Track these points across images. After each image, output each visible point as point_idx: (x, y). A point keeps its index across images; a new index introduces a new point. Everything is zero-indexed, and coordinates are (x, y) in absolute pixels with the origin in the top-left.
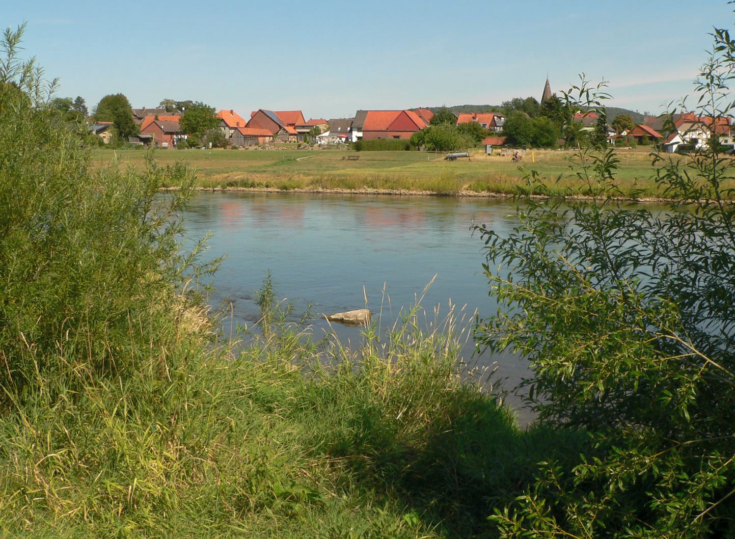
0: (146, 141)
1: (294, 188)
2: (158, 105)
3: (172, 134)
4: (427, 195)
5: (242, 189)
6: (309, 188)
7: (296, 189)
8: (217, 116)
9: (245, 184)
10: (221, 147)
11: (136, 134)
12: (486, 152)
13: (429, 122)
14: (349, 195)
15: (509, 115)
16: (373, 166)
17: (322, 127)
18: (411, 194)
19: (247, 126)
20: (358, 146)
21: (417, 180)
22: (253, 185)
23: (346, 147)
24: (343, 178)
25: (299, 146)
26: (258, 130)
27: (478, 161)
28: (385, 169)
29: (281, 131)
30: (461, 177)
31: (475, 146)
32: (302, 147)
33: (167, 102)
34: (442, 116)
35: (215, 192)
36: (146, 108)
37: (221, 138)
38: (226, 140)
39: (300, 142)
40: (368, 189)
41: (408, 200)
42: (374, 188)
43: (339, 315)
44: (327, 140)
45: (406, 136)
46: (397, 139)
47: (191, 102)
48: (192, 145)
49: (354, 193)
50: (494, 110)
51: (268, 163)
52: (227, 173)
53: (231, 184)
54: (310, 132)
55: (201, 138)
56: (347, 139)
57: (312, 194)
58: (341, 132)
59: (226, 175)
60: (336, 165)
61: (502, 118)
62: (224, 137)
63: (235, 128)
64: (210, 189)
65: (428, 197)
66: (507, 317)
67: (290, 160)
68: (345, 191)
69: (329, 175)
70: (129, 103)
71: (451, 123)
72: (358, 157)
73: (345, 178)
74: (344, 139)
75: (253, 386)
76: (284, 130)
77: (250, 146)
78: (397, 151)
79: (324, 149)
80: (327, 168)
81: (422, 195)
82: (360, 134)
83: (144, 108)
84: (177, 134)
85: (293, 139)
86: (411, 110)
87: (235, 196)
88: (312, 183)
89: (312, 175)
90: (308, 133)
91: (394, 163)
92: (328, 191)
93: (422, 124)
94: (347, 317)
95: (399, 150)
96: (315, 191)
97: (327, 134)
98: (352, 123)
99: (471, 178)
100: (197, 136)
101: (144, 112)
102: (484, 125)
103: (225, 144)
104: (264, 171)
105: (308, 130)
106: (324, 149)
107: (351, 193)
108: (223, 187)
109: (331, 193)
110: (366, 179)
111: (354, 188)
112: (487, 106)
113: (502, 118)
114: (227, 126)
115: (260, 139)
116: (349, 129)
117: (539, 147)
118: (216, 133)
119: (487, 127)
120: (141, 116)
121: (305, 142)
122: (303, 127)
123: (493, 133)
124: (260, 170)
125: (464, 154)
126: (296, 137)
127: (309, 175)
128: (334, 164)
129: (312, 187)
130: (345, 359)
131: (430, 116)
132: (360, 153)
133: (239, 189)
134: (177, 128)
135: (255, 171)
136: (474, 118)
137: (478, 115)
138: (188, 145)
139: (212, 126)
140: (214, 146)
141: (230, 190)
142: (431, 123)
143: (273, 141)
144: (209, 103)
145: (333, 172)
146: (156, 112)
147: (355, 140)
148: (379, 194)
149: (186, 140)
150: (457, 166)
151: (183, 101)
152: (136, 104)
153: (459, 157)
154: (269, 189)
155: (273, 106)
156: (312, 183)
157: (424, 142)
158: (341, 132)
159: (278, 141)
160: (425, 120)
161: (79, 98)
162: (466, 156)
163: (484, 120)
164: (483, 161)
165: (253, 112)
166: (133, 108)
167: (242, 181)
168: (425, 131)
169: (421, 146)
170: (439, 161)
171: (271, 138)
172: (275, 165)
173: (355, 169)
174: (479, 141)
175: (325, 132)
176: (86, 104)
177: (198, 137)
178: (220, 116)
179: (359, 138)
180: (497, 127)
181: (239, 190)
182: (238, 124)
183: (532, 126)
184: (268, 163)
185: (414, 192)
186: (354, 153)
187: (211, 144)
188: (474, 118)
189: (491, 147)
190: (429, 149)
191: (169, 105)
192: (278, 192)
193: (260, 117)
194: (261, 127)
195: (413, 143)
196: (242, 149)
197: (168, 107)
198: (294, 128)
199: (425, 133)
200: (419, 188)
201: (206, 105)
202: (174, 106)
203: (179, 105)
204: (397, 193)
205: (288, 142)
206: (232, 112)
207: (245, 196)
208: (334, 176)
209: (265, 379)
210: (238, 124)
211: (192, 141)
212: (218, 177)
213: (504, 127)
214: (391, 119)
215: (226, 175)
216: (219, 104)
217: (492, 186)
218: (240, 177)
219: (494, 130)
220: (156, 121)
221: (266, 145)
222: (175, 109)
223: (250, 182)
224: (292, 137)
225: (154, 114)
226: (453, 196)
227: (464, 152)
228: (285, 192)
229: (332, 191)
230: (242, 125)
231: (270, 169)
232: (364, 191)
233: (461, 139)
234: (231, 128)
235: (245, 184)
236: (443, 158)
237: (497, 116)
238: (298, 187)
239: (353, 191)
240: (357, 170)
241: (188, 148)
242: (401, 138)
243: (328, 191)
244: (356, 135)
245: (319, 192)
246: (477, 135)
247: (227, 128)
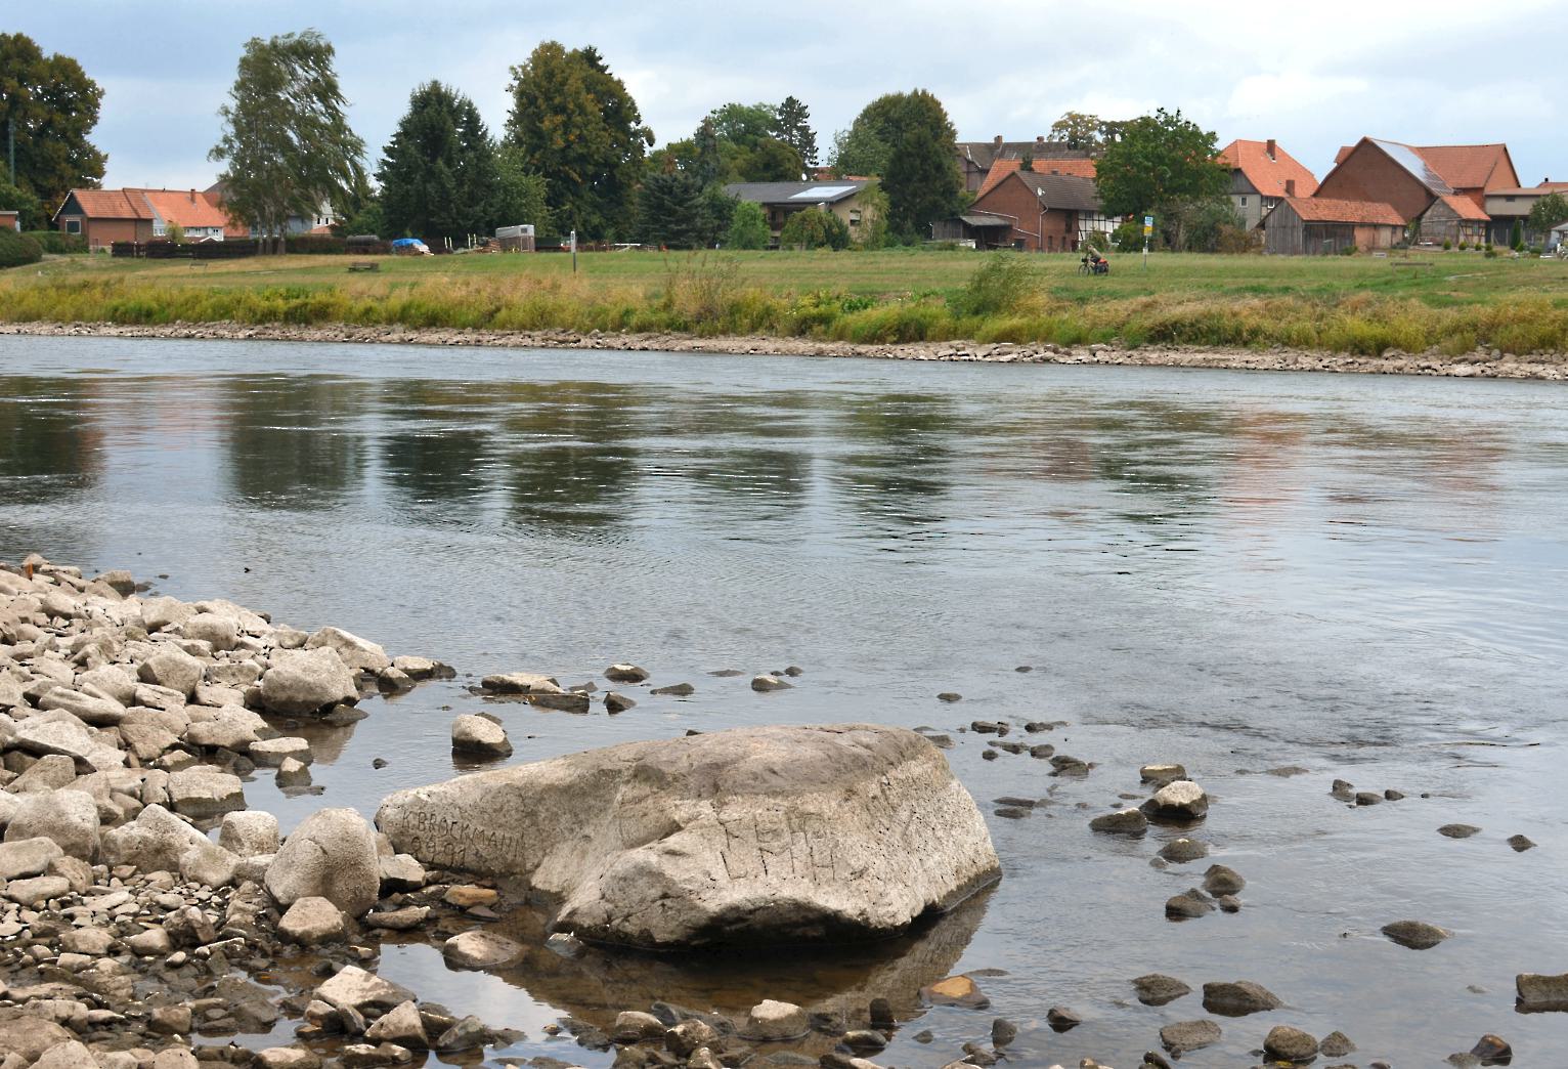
11: (953, 214)
19: (1326, 189)
26: (1353, 205)
33: (1076, 120)
70: (949, 119)
83: (998, 139)
101: (997, 149)
117: (1233, 252)
152: (971, 121)
161: (791, 101)
165: (1343, 149)
166: (960, 139)
176: (813, 123)
178: (1231, 160)
193: (1364, 165)
194: (1367, 197)
201: (952, 125)
216: (1228, 117)
230: (1303, 191)
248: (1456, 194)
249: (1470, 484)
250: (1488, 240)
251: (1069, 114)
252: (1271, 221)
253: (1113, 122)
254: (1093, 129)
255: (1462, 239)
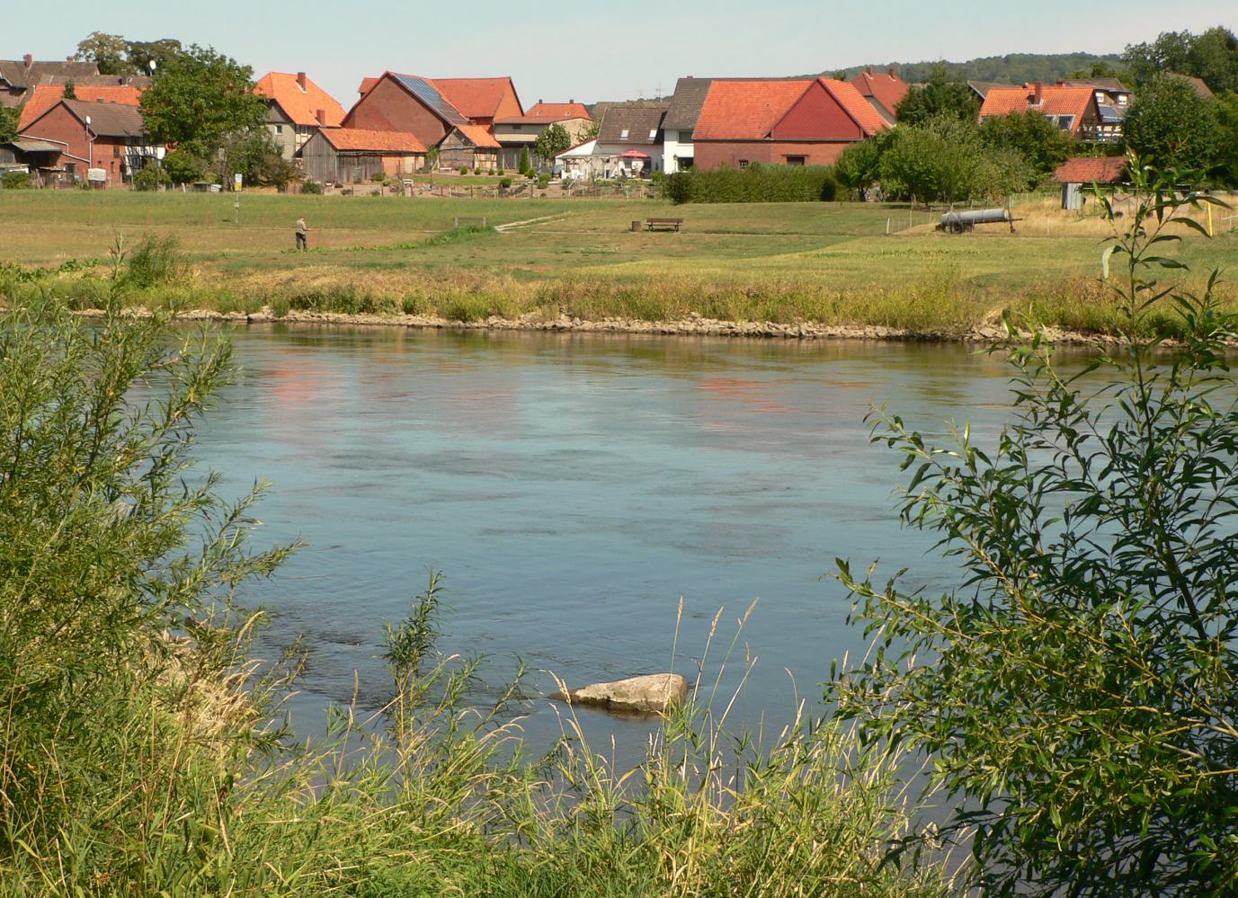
0: (40, 161)
1: (487, 315)
2: (73, 51)
3: (117, 141)
4: (879, 339)
5: (332, 316)
6: (529, 316)
7: (493, 320)
8: (256, 92)
9: (344, 302)
10: (269, 184)
12: (1064, 206)
13: (893, 111)
14: (646, 337)
15: (1145, 87)
16: (721, 249)
17: (573, 128)
18: (831, 337)
19: (348, 121)
20: (679, 190)
21: (849, 295)
22: (368, 306)
23: (644, 189)
24: (629, 287)
25: (505, 184)
26: (381, 134)
27: (1038, 233)
28: (755, 261)
29: (451, 140)
30: (980, 284)
31: (1033, 186)
32: (513, 187)
33: (101, 41)
34: (937, 94)
35: (252, 326)
36: (35, 59)
37: (270, 159)
38: (283, 165)
39: (508, 173)
40: (706, 321)
41: (821, 353)
42: (721, 318)
43: (599, 690)
44: (587, 167)
45: (824, 158)
46: (797, 168)
47: (177, 44)
48: (179, 177)
49: (664, 333)
50: (1097, 69)
51: (412, 237)
52: (289, 268)
53: (301, 303)
54: (534, 145)
55: (207, 156)
56: (647, 164)
57: (539, 334)
58: (629, 144)
59: (285, 275)
60: (613, 248)
61: (1122, 98)
62: (279, 154)
63: (313, 130)
64: (239, 316)
65: (882, 344)
66: (896, 672)
67: (477, 231)
68: (636, 325)
69: (590, 279)
71: (962, 116)
72: (679, 221)
73: (634, 287)
74: (638, 165)
75: (360, 862)
76: (460, 135)
77: (358, 182)
78: (797, 204)
79: (579, 193)
80: (586, 259)
81: (865, 338)
82: (688, 151)
83: (28, 57)
84: (134, 141)
85: (487, 163)
86: (841, 76)
87: (307, 340)
88: (541, 301)
89: (539, 277)
90: (531, 145)
91: (784, 239)
92: (588, 325)
93: (875, 119)
94: (622, 695)
95: (802, 199)
96: (549, 324)
97: (588, 148)
98: (664, 115)
99: (1010, 287)
100: (195, 152)
102: (1064, 121)
103: (279, 180)
104: (400, 265)
105: (532, 138)
106: (579, 193)
107: (654, 333)
108: (279, 310)
109: (596, 331)
110: (698, 291)
111: (662, 317)
112: (1081, 58)
113: (1122, 98)
114: (289, 120)
115: (389, 163)
116: (653, 133)
118: (253, 143)
119: (1073, 125)
120: (18, 84)
121: (521, 173)
122: (517, 127)
123: (1090, 146)
124: (387, 261)
125: (996, 212)
126: (494, 157)
127: (530, 277)
128: (605, 244)
129: (539, 312)
130: (595, 792)
131: (896, 93)
132: (685, 210)
133: (324, 316)
134: (135, 124)
135: (373, 265)
136: (1032, 99)
137: (1045, 90)
138: (169, 178)
139: (238, 122)
140: (248, 182)
141: (297, 321)
142: (900, 117)
143: (426, 169)
144: (234, 46)
145: (602, 270)
146: (68, 72)
147: (670, 167)
148: (737, 335)
149: (162, 161)
150: (972, 248)
151: (152, 40)
153: (980, 221)
154: (416, 320)
155: (425, 64)
156: (541, 301)
157: (877, 177)
158: (629, 144)
159: (442, 169)
160: (881, 107)
162: (1002, 219)
163: (1065, 104)
164: (1054, 235)
165: (366, 81)
167: (335, 292)
168: (881, 140)
169: (870, 185)
170: (920, 235)
171: (421, 159)
172: (432, 244)
173: (664, 261)
174: (1047, 169)
175: (584, 142)
177: (197, 153)
179: (685, 162)
180: (1104, 125)
181: (318, 323)
182: (320, 115)
183: (1214, 121)
184: (412, 237)
185: (838, 331)
186: (668, 210)
187: (239, 178)
188: (1032, 99)
189: (1081, 190)
190: (893, 197)
191: (107, 51)
192: (439, 327)
193: (388, 95)
194: (391, 128)
195: (843, 178)
196: (332, 192)
197: (105, 59)
198: (491, 131)
199: (881, 149)
200: (855, 316)
201: (223, 58)
202: (124, 57)
203: (140, 55)
204: (789, 331)
205: (470, 174)
206: (301, 78)
207: (347, 340)
208: (604, 280)
209: (391, 846)
210: (320, 115)
211: (181, 164)
212: (258, 281)
213: (1126, 126)
214: (779, 105)
215: (285, 275)
216: (262, 57)
217: (1076, 311)
218: (326, 280)
219: (1096, 135)
220: (67, 101)
221: (406, 181)
222: (124, 64)
223: (359, 297)
224: (483, 157)
225: (63, 79)
226: (955, 341)
227: (999, 205)
228: (462, 329)
229: (599, 325)
230: (334, 119)
231: (416, 257)
232: (691, 327)
233: (987, 167)
234: (299, 129)
235: (344, 302)
236: (933, 225)
237: (1106, 92)
238: (500, 314)
239: (659, 325)
240: (674, 262)
241: (168, 186)
242: (809, 163)
243: (588, 325)
244: (674, 152)
245: (561, 330)
246: (1038, 150)
247: (286, 128)
248: (470, 123)
249: (1098, 375)
250: (499, 165)
251: (95, 34)
252: (307, 151)
253: (138, 43)
254: (119, 49)
255: (477, 165)
